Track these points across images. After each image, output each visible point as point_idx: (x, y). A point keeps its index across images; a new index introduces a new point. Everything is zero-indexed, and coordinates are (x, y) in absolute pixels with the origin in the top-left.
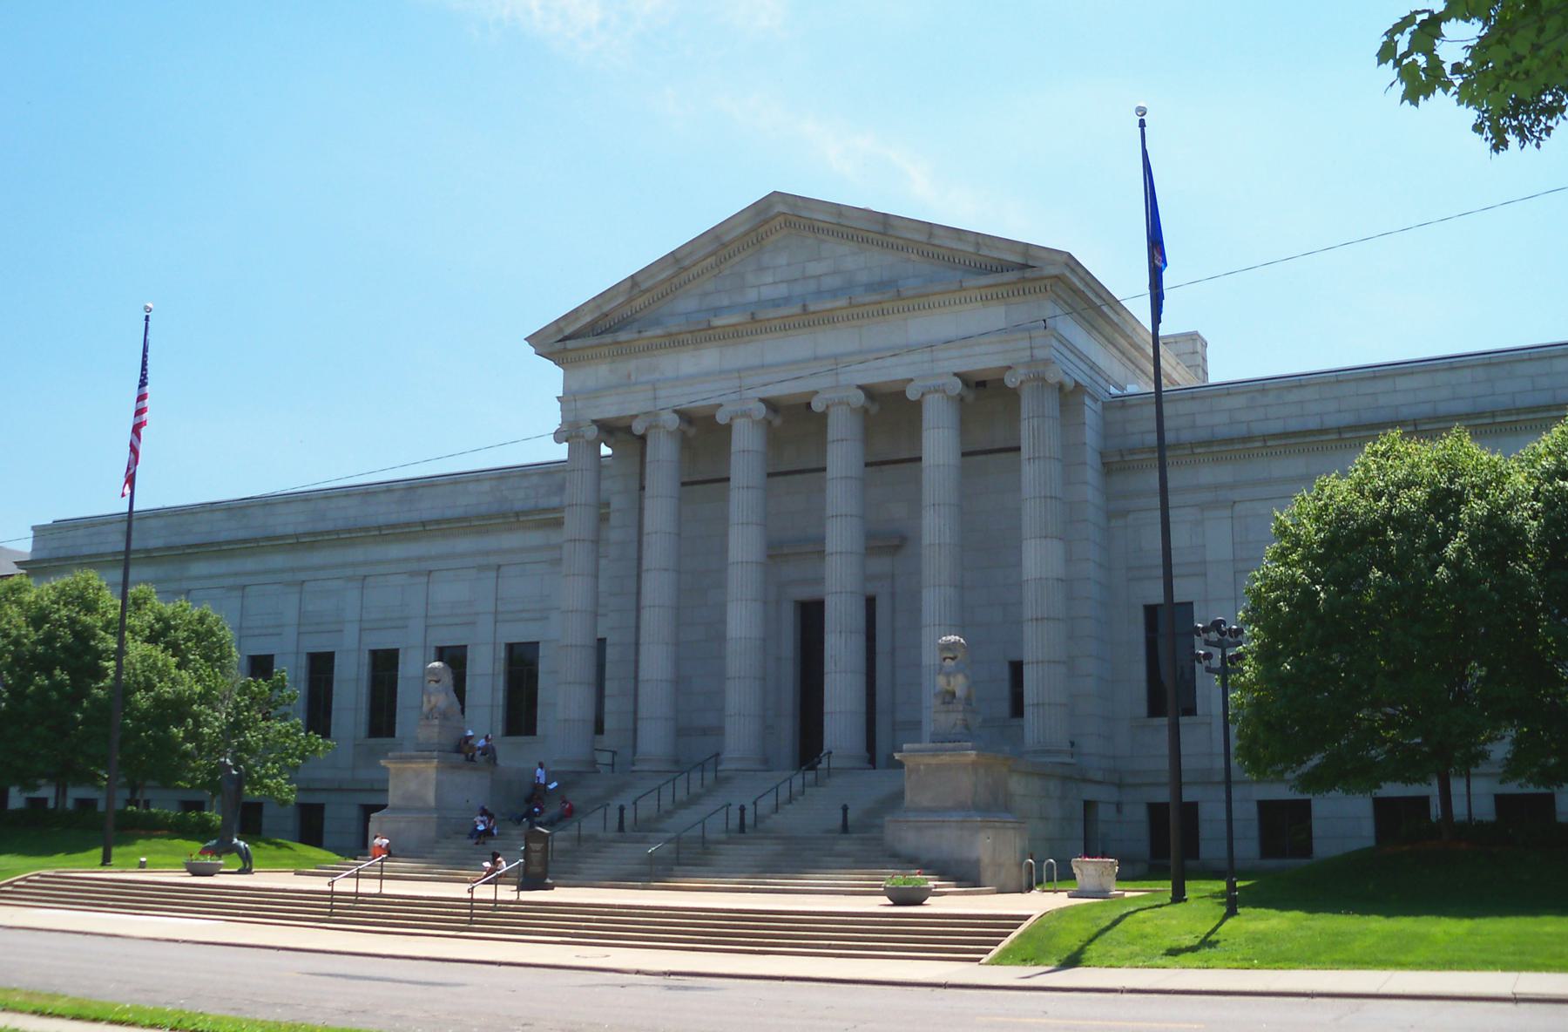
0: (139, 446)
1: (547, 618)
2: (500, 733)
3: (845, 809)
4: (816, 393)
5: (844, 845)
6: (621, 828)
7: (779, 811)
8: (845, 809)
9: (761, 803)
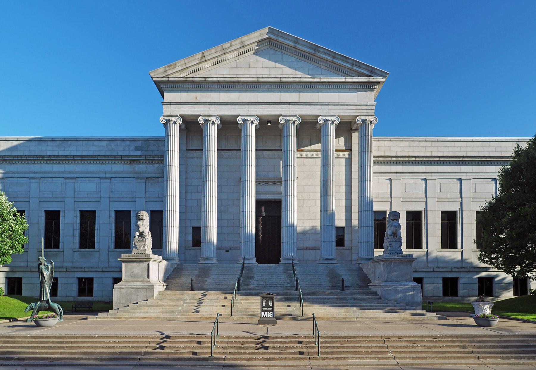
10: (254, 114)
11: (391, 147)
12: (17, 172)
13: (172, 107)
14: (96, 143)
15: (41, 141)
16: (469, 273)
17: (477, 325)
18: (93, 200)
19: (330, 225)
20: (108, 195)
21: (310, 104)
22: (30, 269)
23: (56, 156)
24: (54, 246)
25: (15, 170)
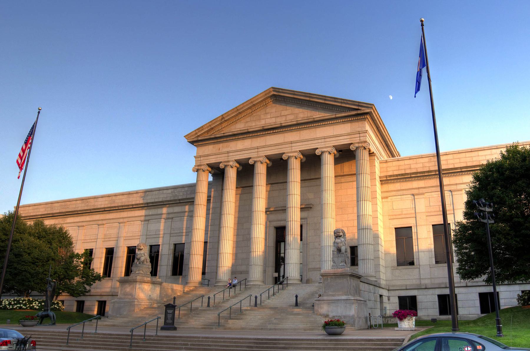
0: (355, 154)
1: (188, 235)
2: (169, 275)
3: (297, 297)
4: (250, 158)
5: (297, 310)
6: (208, 305)
7: (270, 299)
8: (297, 297)
9: (263, 296)
10: (296, 150)
11: (411, 165)
12: (113, 219)
13: (202, 158)
14: (165, 191)
15: (130, 195)
16: (509, 286)
17: (422, 342)
18: (175, 235)
19: (327, 245)
20: (169, 232)
21: (308, 140)
22: (466, 284)
23: (445, 169)
24: (108, 276)
25: (111, 217)
